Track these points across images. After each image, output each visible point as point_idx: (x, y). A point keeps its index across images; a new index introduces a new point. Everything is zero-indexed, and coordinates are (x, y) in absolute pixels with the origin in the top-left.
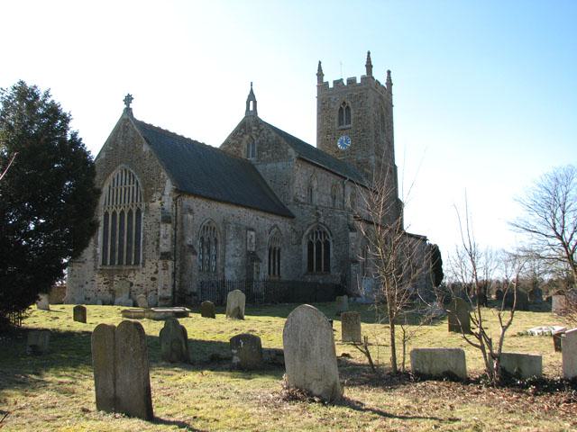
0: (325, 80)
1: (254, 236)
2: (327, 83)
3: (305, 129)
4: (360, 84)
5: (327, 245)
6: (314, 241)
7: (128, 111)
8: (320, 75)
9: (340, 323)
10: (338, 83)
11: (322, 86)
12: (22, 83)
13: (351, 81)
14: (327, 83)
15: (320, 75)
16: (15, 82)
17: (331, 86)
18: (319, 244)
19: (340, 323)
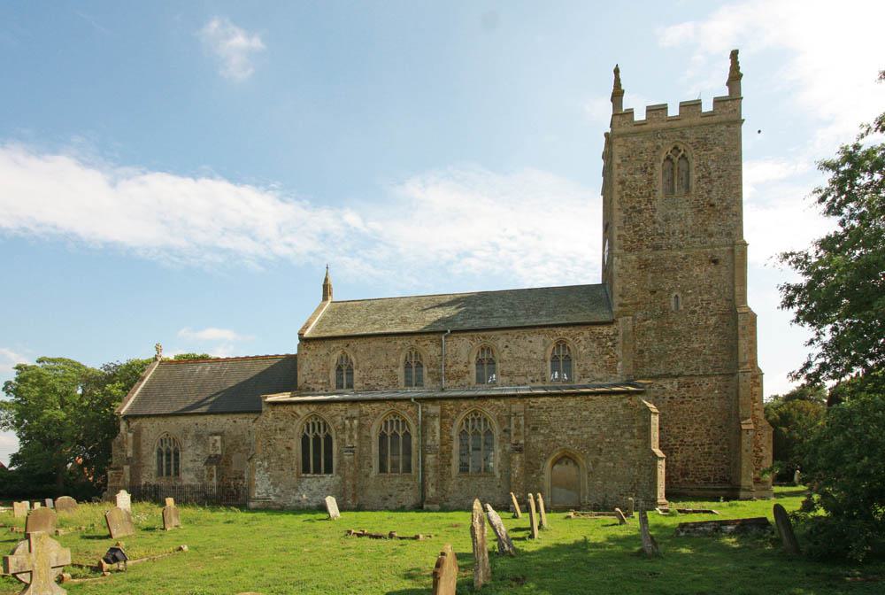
0: (626, 106)
1: (496, 545)
2: (630, 112)
3: (832, 226)
4: (641, 124)
5: (328, 439)
6: (311, 436)
7: (54, 501)
8: (617, 95)
9: (172, 499)
10: (656, 111)
11: (621, 115)
12: (113, 184)
13: (691, 107)
14: (630, 112)
15: (617, 95)
16: (878, 73)
17: (640, 116)
18: (317, 439)
19: (172, 499)
